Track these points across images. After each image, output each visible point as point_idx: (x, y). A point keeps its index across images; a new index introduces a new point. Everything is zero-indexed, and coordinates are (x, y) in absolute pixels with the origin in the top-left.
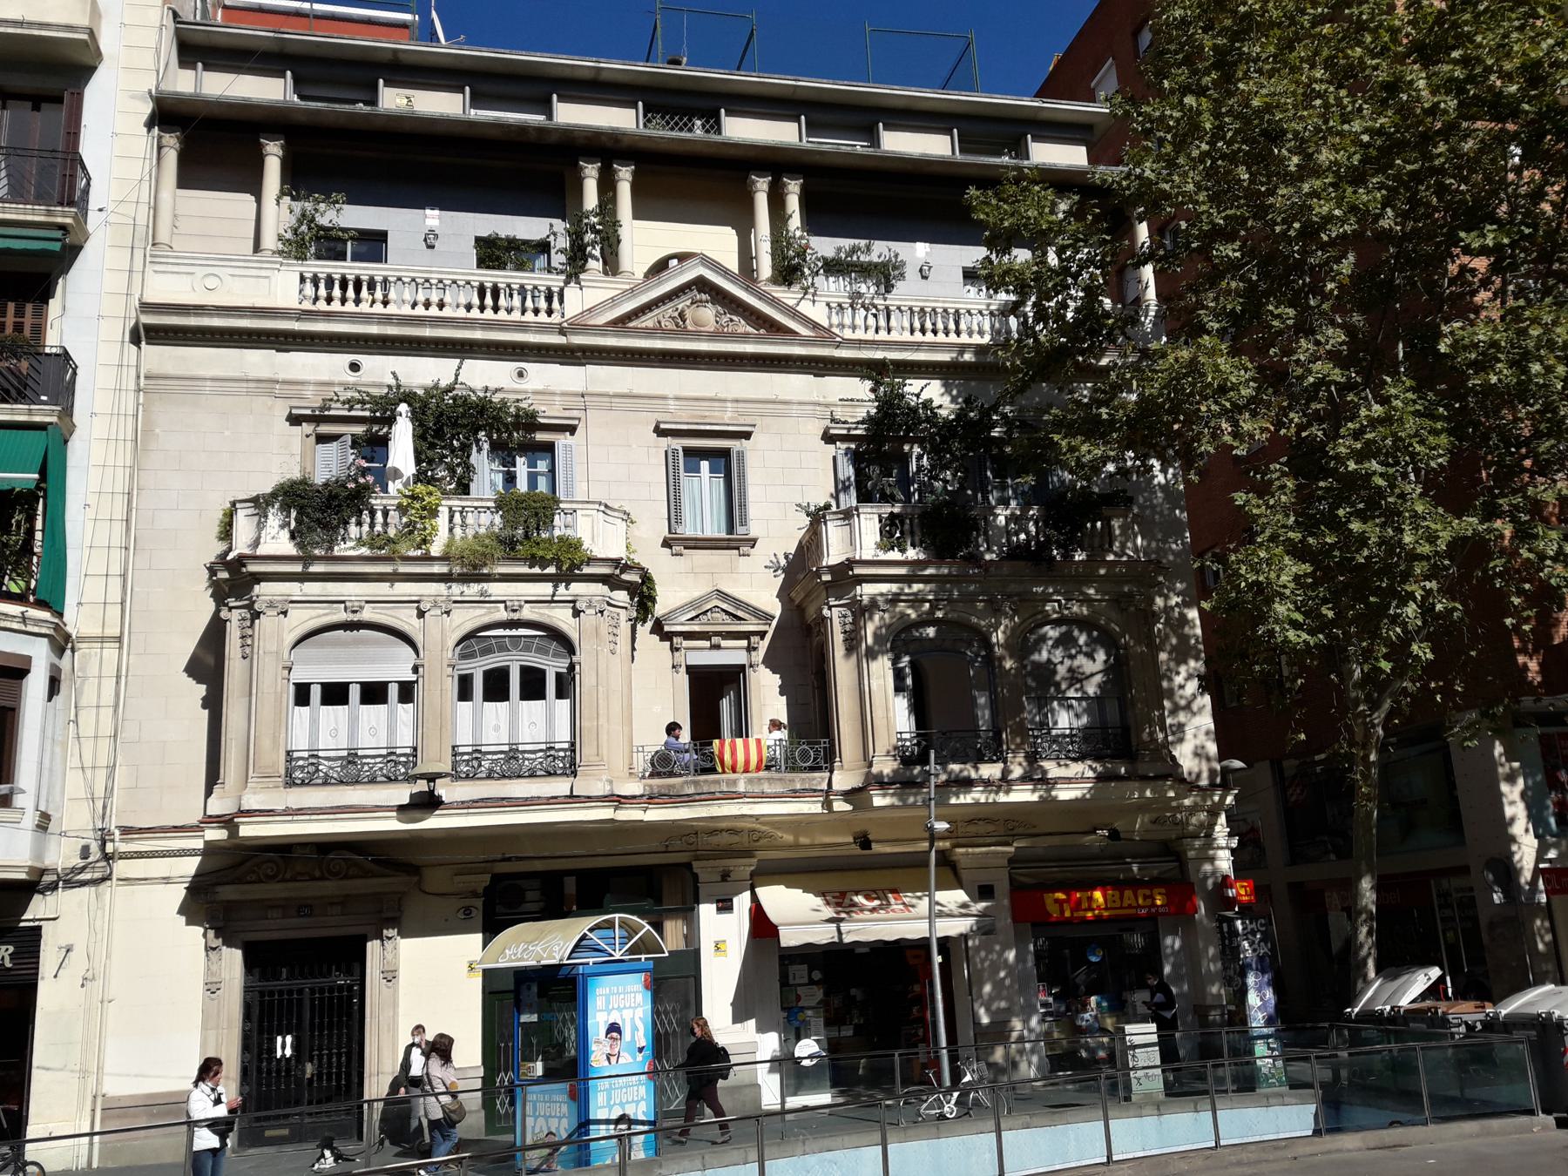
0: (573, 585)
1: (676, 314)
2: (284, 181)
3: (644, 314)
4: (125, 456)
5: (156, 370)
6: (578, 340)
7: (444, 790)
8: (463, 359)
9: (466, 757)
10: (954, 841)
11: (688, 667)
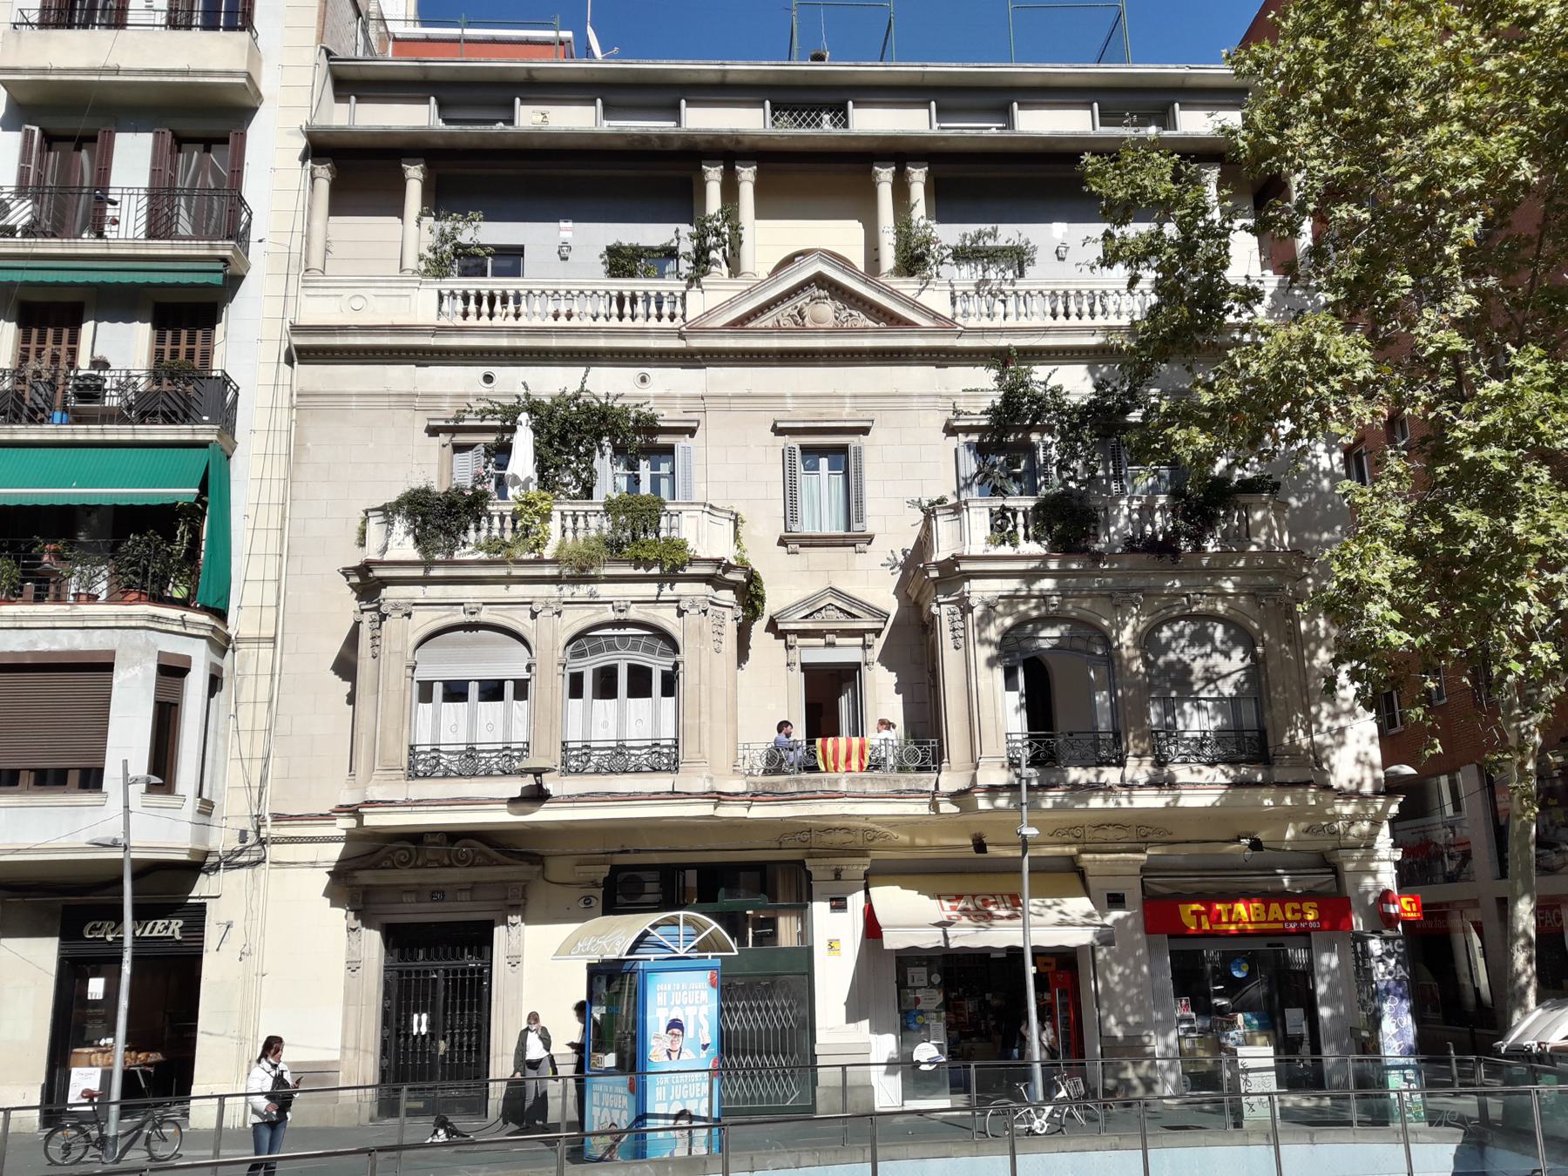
0: (677, 585)
1: (795, 312)
2: (424, 203)
3: (763, 313)
4: (279, 470)
5: (308, 388)
6: (696, 343)
7: (551, 784)
8: (589, 366)
9: (575, 753)
10: (1081, 846)
11: (803, 665)
